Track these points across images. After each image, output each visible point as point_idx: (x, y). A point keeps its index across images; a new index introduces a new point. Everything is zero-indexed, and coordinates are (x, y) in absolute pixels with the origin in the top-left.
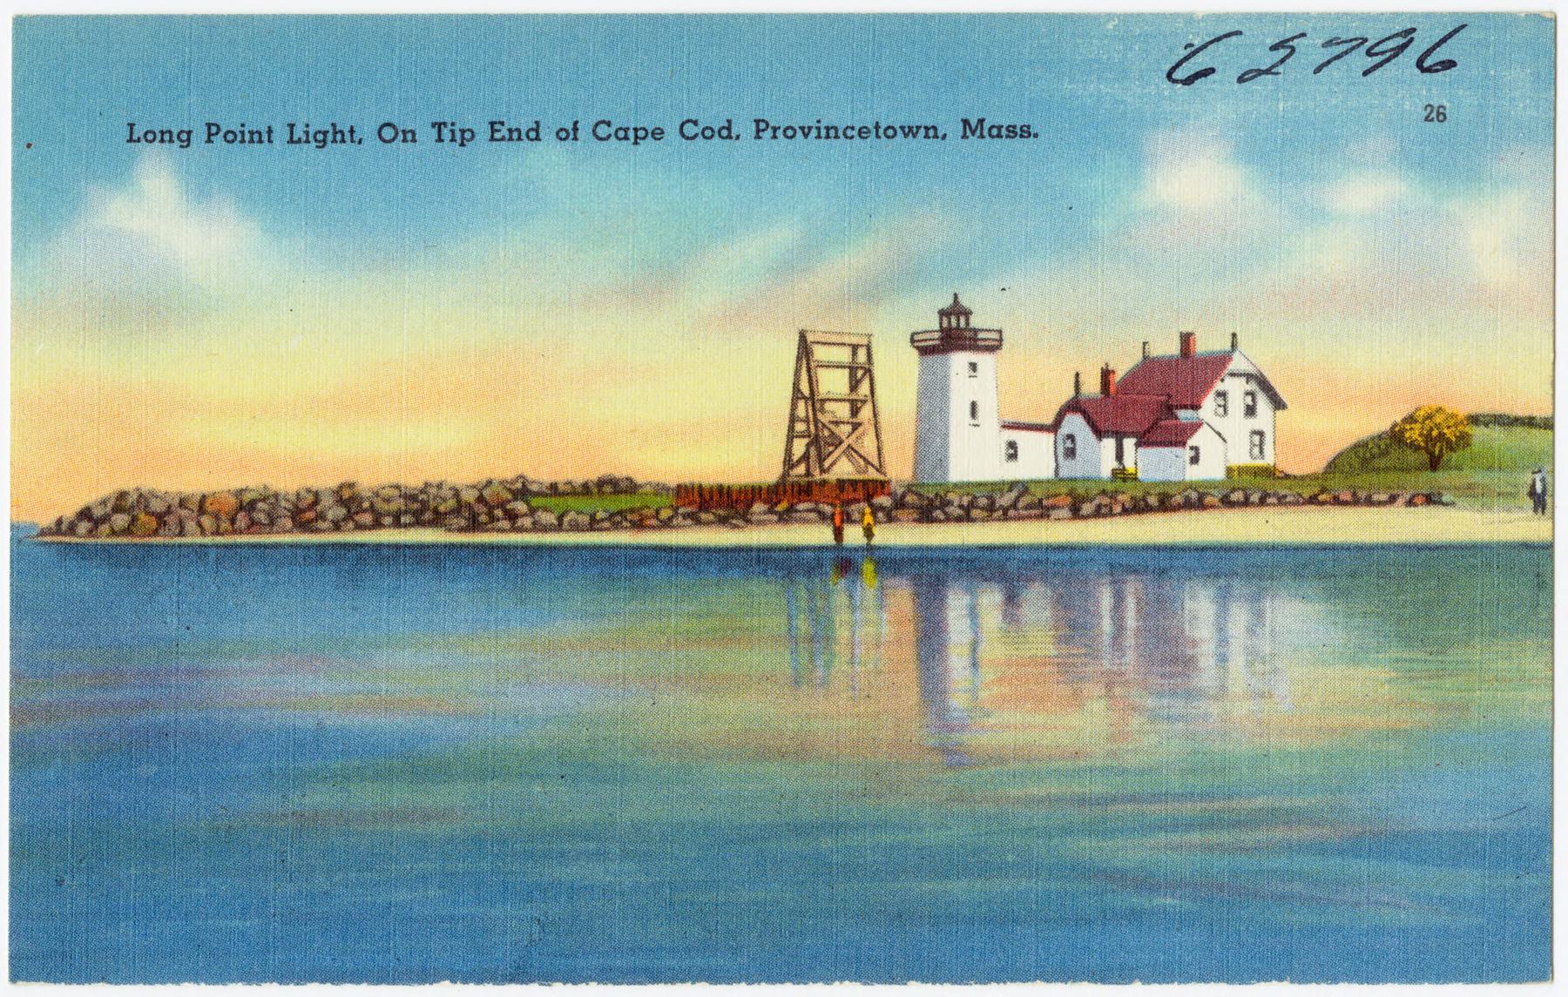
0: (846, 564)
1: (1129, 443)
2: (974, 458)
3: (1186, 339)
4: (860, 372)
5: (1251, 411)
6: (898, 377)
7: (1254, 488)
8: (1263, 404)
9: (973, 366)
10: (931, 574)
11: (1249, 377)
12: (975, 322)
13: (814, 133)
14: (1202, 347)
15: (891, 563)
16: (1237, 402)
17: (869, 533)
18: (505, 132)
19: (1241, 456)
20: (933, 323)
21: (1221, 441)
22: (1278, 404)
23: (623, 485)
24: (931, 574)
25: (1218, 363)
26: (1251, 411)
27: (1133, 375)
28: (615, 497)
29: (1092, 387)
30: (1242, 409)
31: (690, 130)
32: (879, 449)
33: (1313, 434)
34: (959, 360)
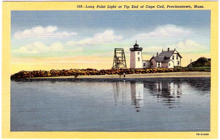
0: (121, 81)
1: (161, 63)
2: (139, 65)
3: (169, 49)
4: (123, 53)
5: (177, 58)
6: (128, 55)
7: (177, 69)
8: (179, 58)
9: (139, 53)
10: (133, 82)
11: (177, 54)
12: (139, 47)
13: (175, 7)
14: (170, 50)
15: (127, 81)
16: (175, 58)
17: (124, 76)
18: (134, 7)
19: (176, 65)
20: (133, 47)
21: (172, 64)
22: (181, 57)
23: (54, 81)
24: (133, 82)
25: (173, 52)
26: (177, 58)
27: (161, 54)
28: (90, 72)
29: (155, 56)
30: (176, 58)
31: (158, 7)
32: (126, 64)
33: (185, 64)
34: (136, 52)
